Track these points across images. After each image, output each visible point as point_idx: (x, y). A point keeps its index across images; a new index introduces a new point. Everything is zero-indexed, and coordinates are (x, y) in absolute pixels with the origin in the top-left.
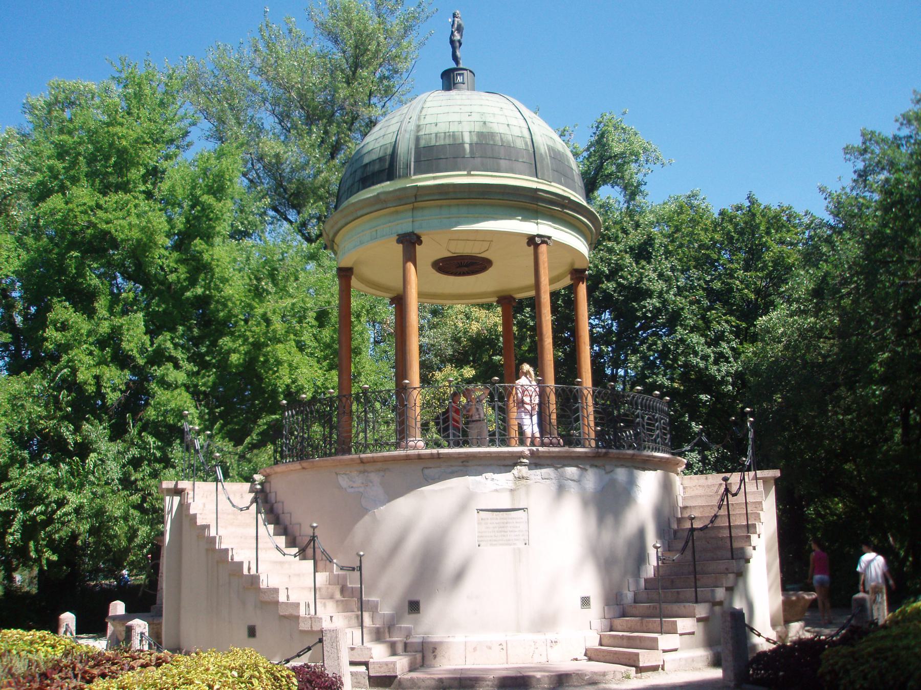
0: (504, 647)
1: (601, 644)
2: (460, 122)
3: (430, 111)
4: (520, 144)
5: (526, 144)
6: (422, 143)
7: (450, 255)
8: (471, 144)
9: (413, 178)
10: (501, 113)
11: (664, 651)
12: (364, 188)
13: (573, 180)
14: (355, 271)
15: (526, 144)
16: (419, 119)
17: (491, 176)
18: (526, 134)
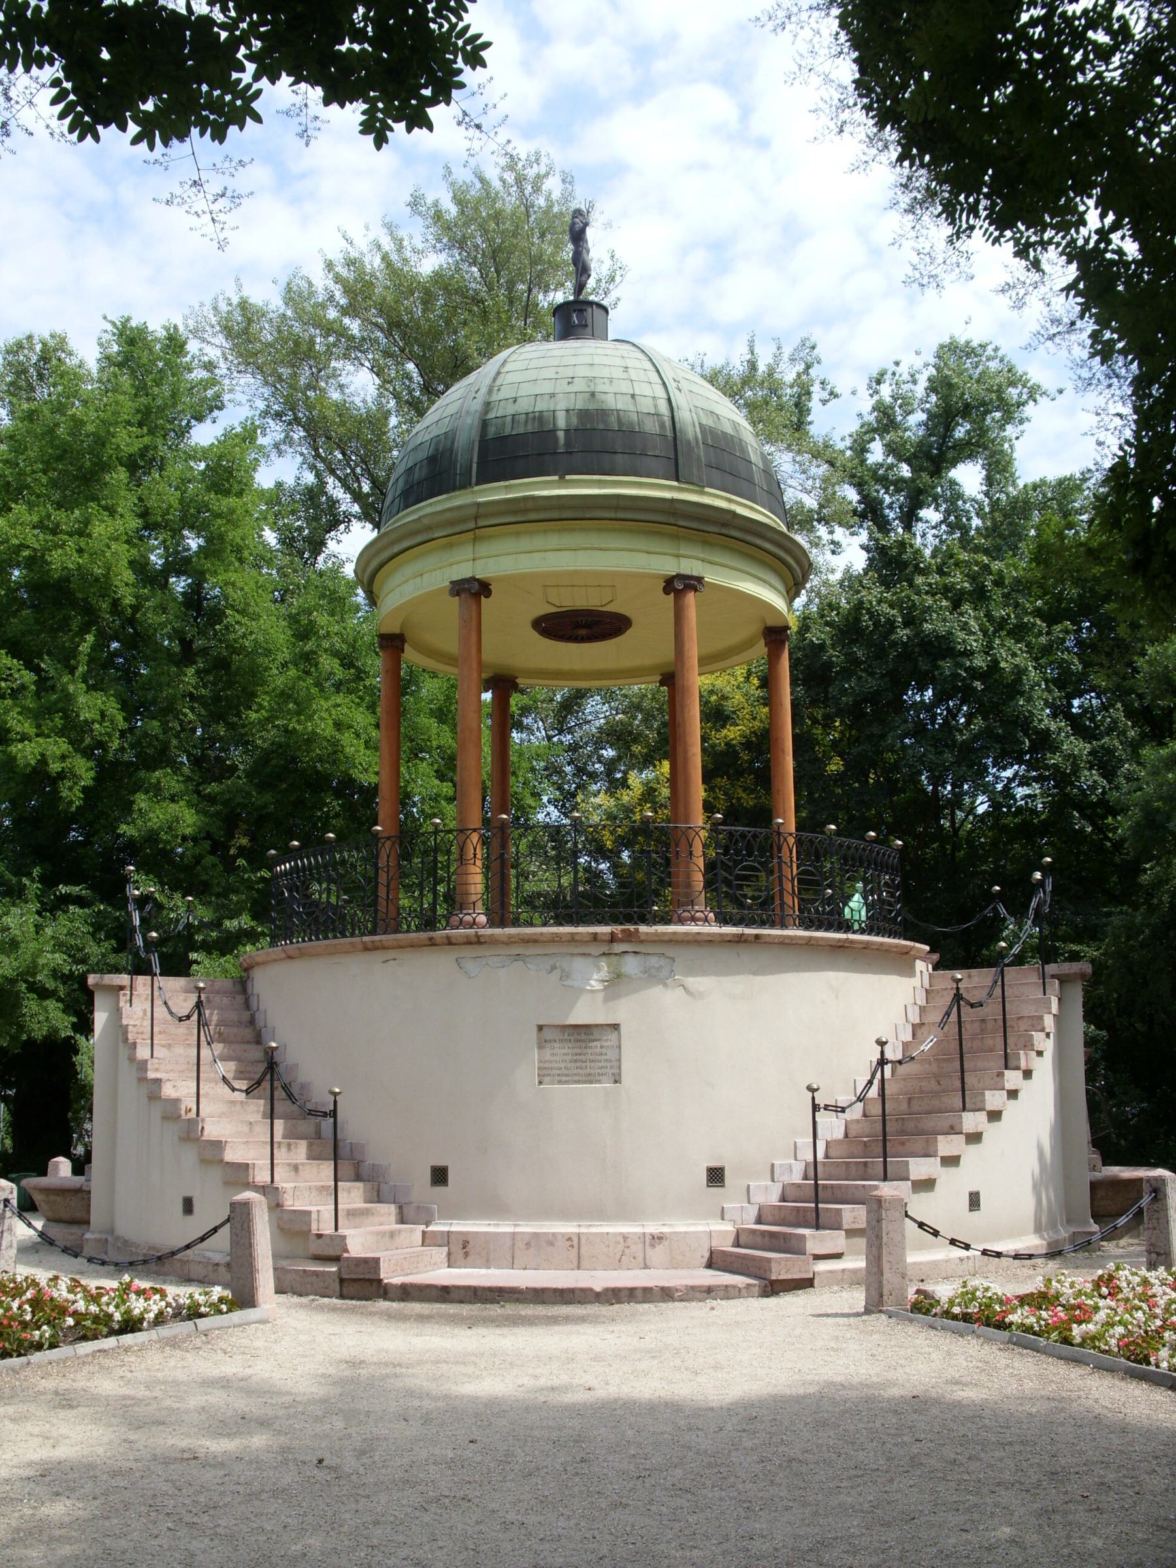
0: (575, 1243)
1: (737, 1244)
2: (552, 395)
3: (510, 378)
4: (651, 427)
5: (662, 425)
6: (492, 432)
7: (554, 610)
8: (567, 431)
9: (477, 488)
10: (625, 375)
11: (818, 1257)
12: (407, 507)
13: (751, 481)
14: (407, 635)
15: (662, 425)
16: (490, 391)
17: (600, 481)
18: (664, 409)
